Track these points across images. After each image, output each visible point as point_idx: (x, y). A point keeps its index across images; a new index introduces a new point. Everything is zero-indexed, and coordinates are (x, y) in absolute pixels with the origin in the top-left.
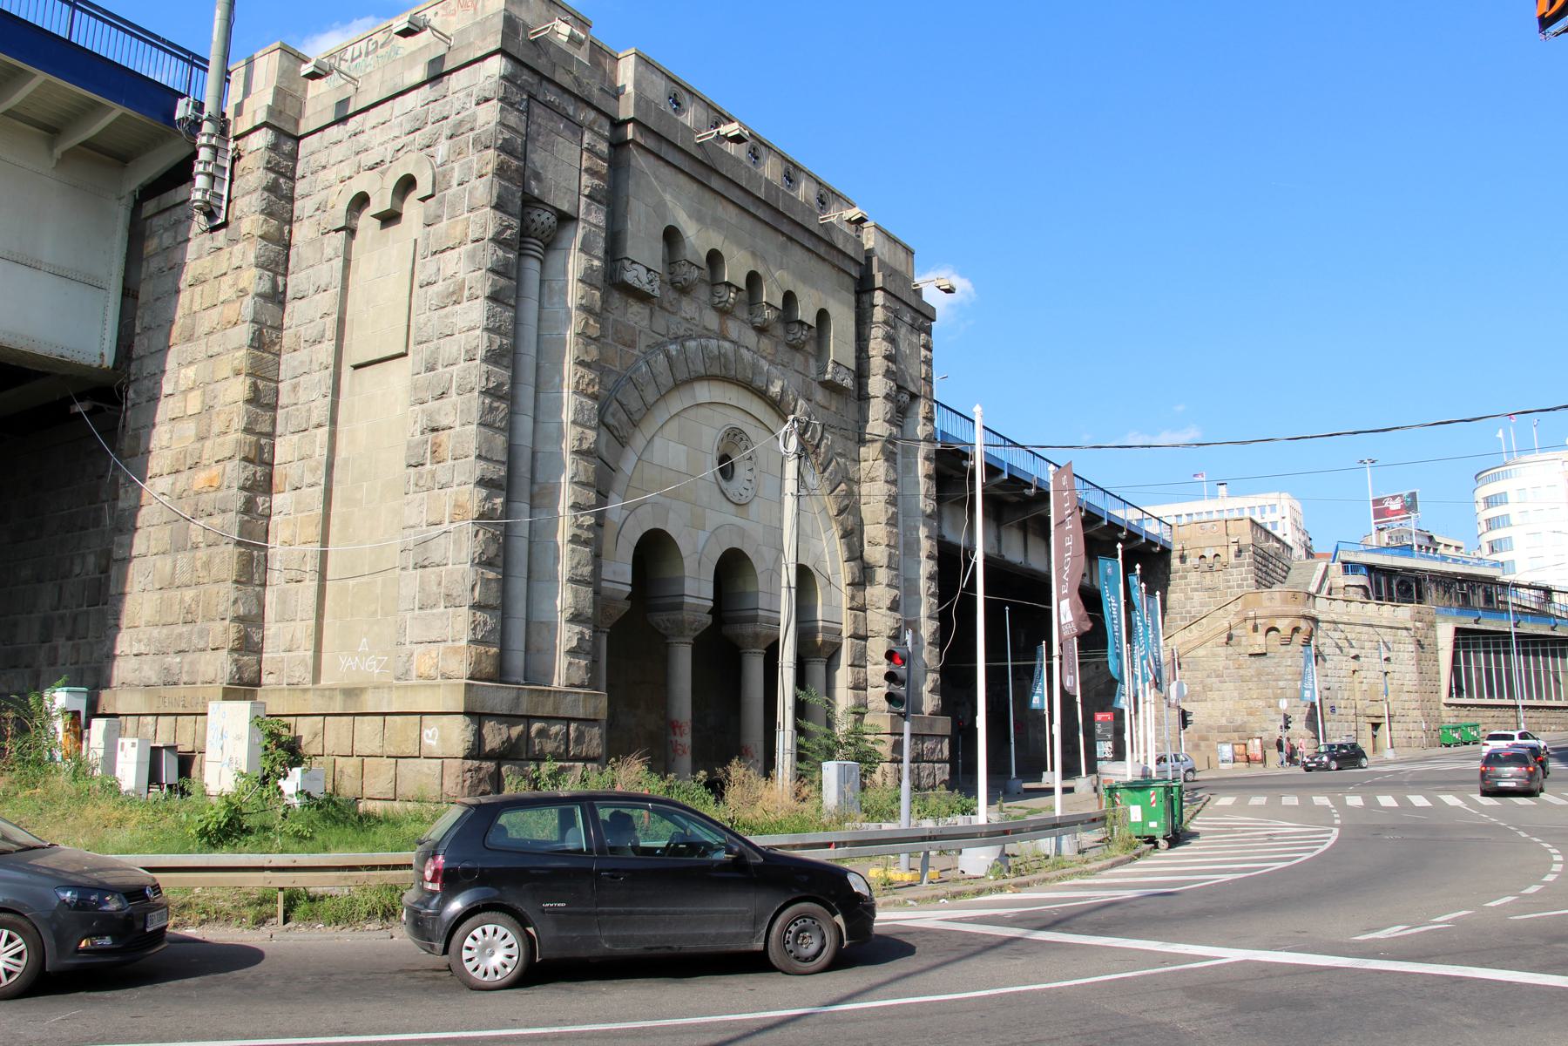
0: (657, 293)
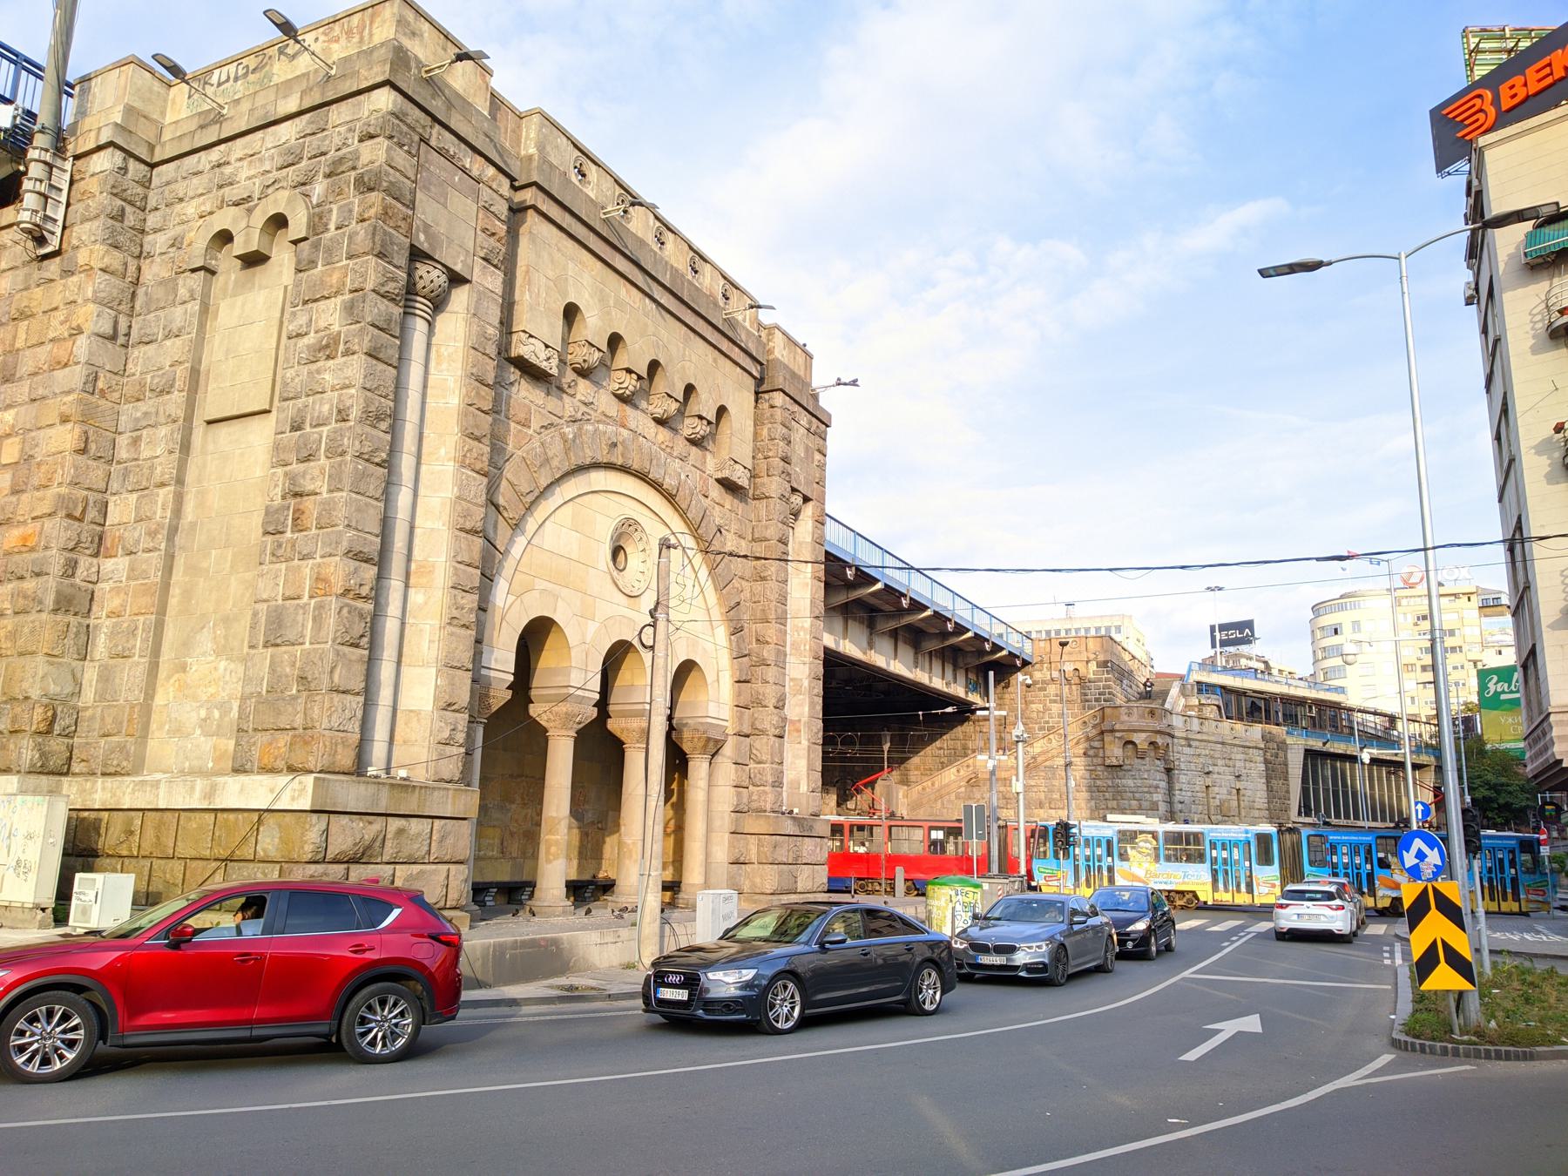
0: (554, 371)
